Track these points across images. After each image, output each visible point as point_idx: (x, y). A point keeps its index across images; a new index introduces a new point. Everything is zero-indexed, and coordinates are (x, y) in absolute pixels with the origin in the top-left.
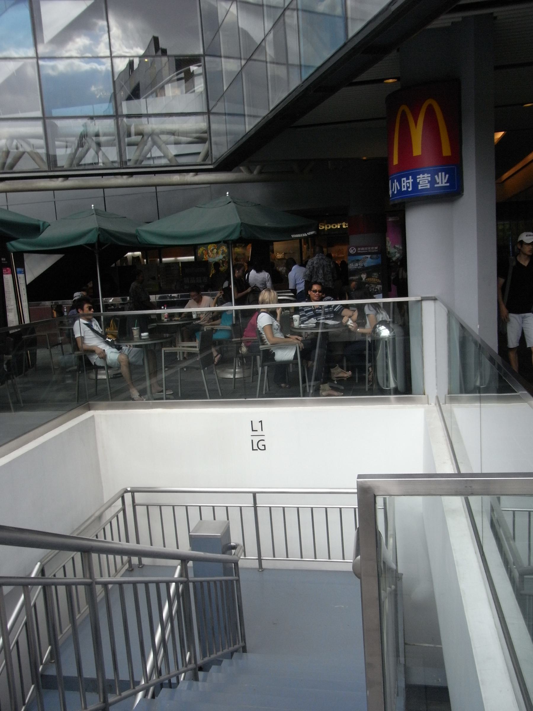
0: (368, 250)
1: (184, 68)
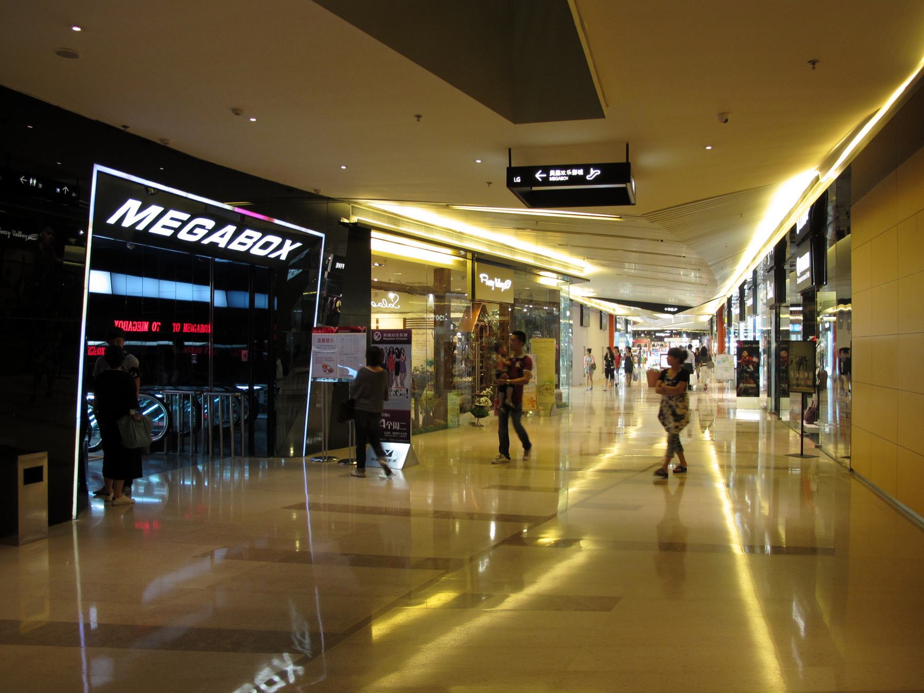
0: (395, 338)
1: (307, 477)
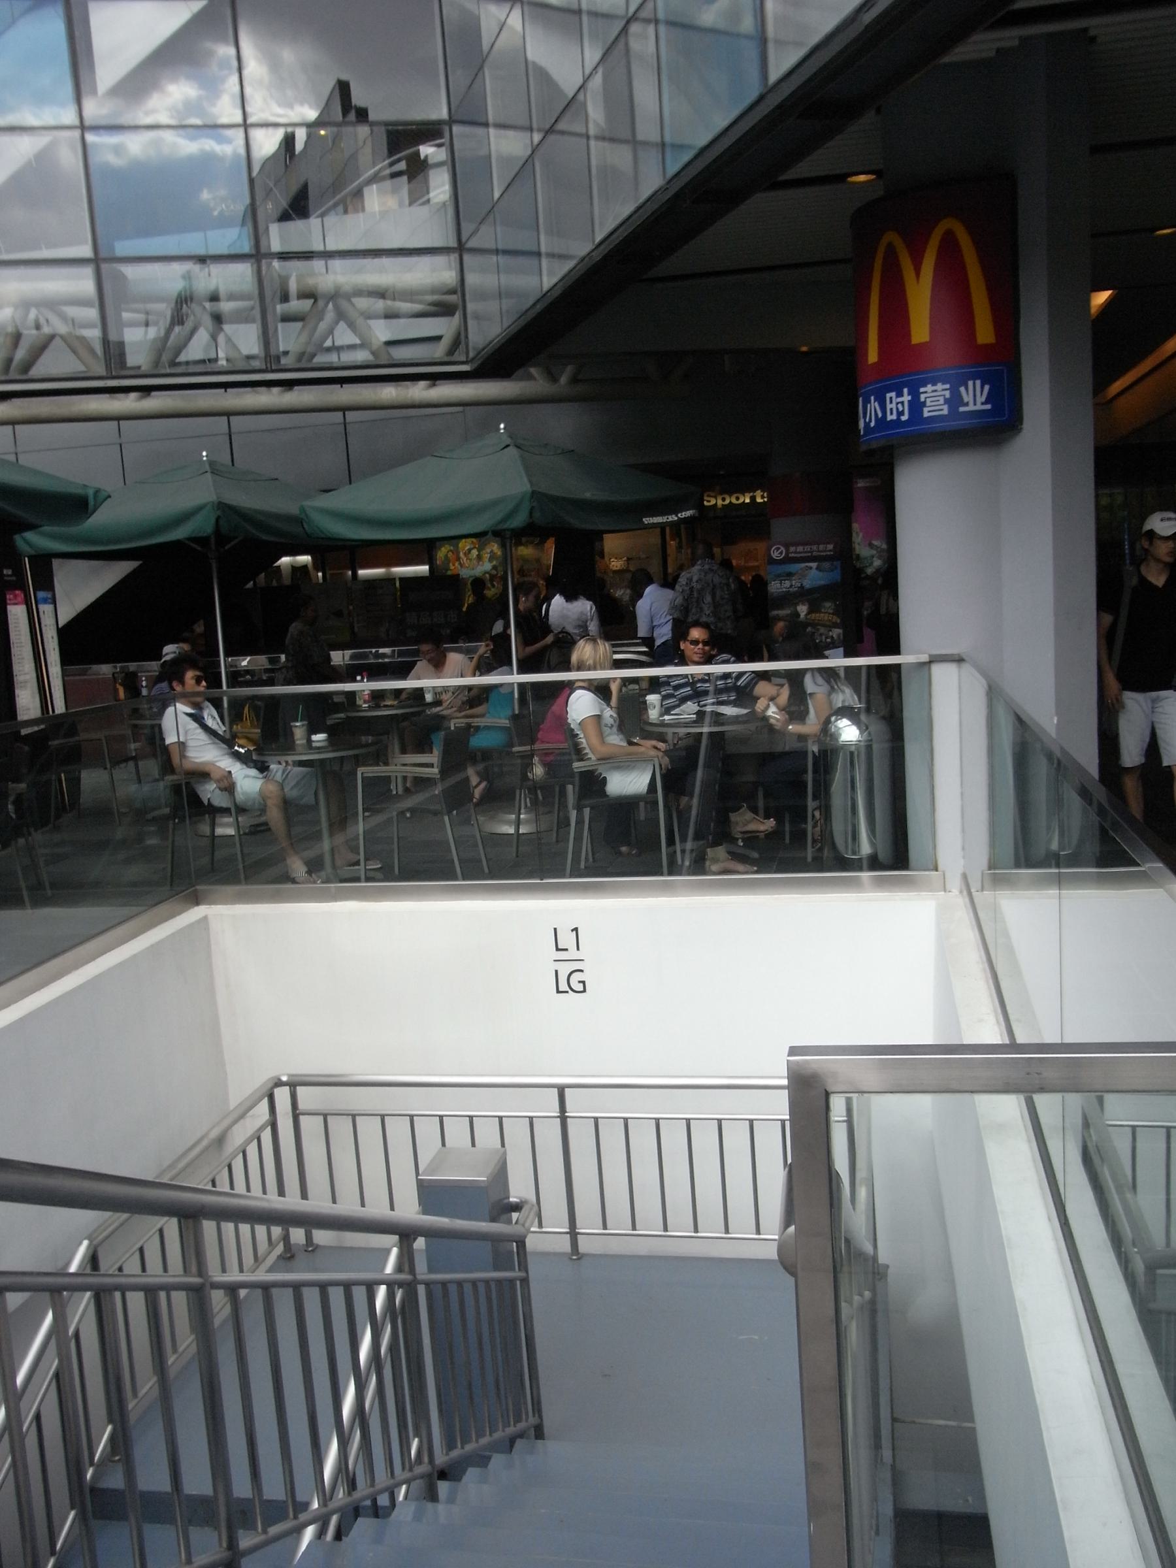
0: (812, 552)
